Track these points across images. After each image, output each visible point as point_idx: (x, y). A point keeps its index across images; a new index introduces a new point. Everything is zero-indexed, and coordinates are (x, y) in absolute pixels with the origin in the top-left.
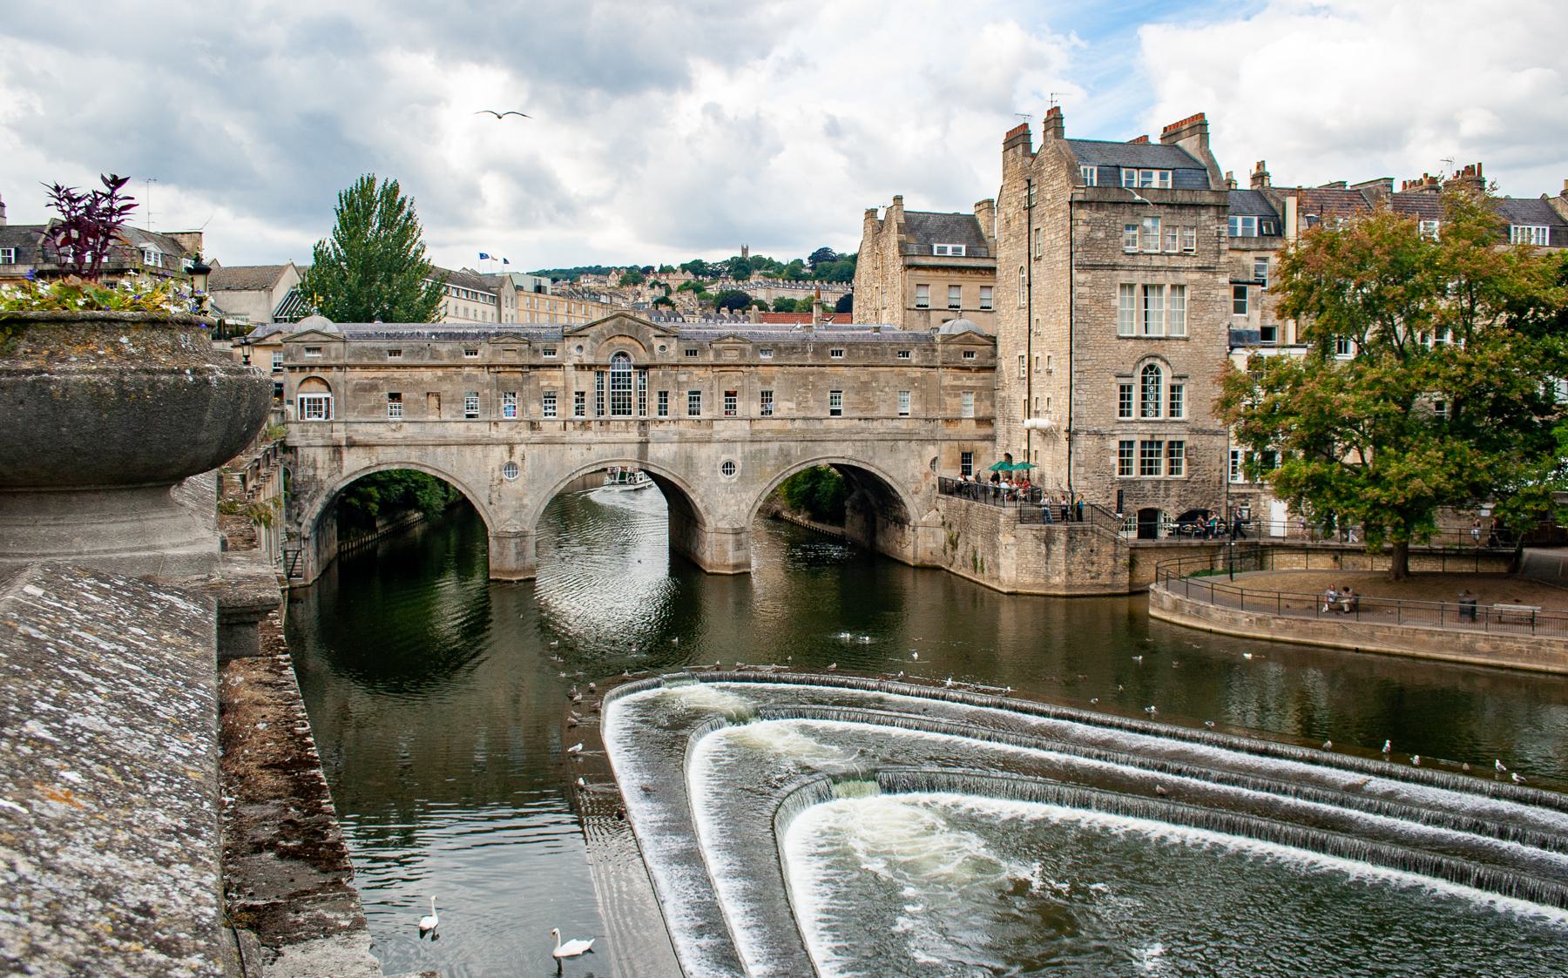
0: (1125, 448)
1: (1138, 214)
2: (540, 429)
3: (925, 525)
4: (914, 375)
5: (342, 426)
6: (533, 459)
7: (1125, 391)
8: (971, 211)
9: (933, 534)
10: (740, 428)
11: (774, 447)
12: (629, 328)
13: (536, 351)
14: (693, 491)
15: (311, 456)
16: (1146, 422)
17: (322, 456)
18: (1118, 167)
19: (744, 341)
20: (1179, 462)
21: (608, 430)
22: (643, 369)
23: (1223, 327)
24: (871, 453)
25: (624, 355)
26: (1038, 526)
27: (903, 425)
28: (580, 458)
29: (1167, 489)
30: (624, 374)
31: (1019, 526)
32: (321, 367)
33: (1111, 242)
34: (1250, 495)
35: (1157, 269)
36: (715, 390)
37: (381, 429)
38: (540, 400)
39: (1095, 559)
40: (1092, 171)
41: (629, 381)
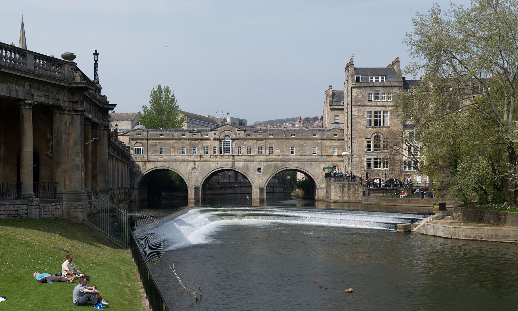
0: (369, 160)
1: (373, 90)
2: (203, 157)
3: (321, 188)
4: (318, 142)
6: (201, 166)
7: (369, 143)
8: (114, 110)
9: (323, 191)
10: (263, 158)
12: (229, 128)
14: (248, 176)
16: (375, 152)
20: (387, 165)
21: (223, 158)
24: (304, 166)
25: (228, 136)
26: (340, 183)
27: (314, 157)
28: (214, 166)
29: (382, 173)
30: (228, 141)
31: (335, 183)
32: (141, 139)
33: (364, 98)
35: (379, 106)
36: (255, 147)
37: (157, 157)
38: (203, 149)
39: (357, 192)
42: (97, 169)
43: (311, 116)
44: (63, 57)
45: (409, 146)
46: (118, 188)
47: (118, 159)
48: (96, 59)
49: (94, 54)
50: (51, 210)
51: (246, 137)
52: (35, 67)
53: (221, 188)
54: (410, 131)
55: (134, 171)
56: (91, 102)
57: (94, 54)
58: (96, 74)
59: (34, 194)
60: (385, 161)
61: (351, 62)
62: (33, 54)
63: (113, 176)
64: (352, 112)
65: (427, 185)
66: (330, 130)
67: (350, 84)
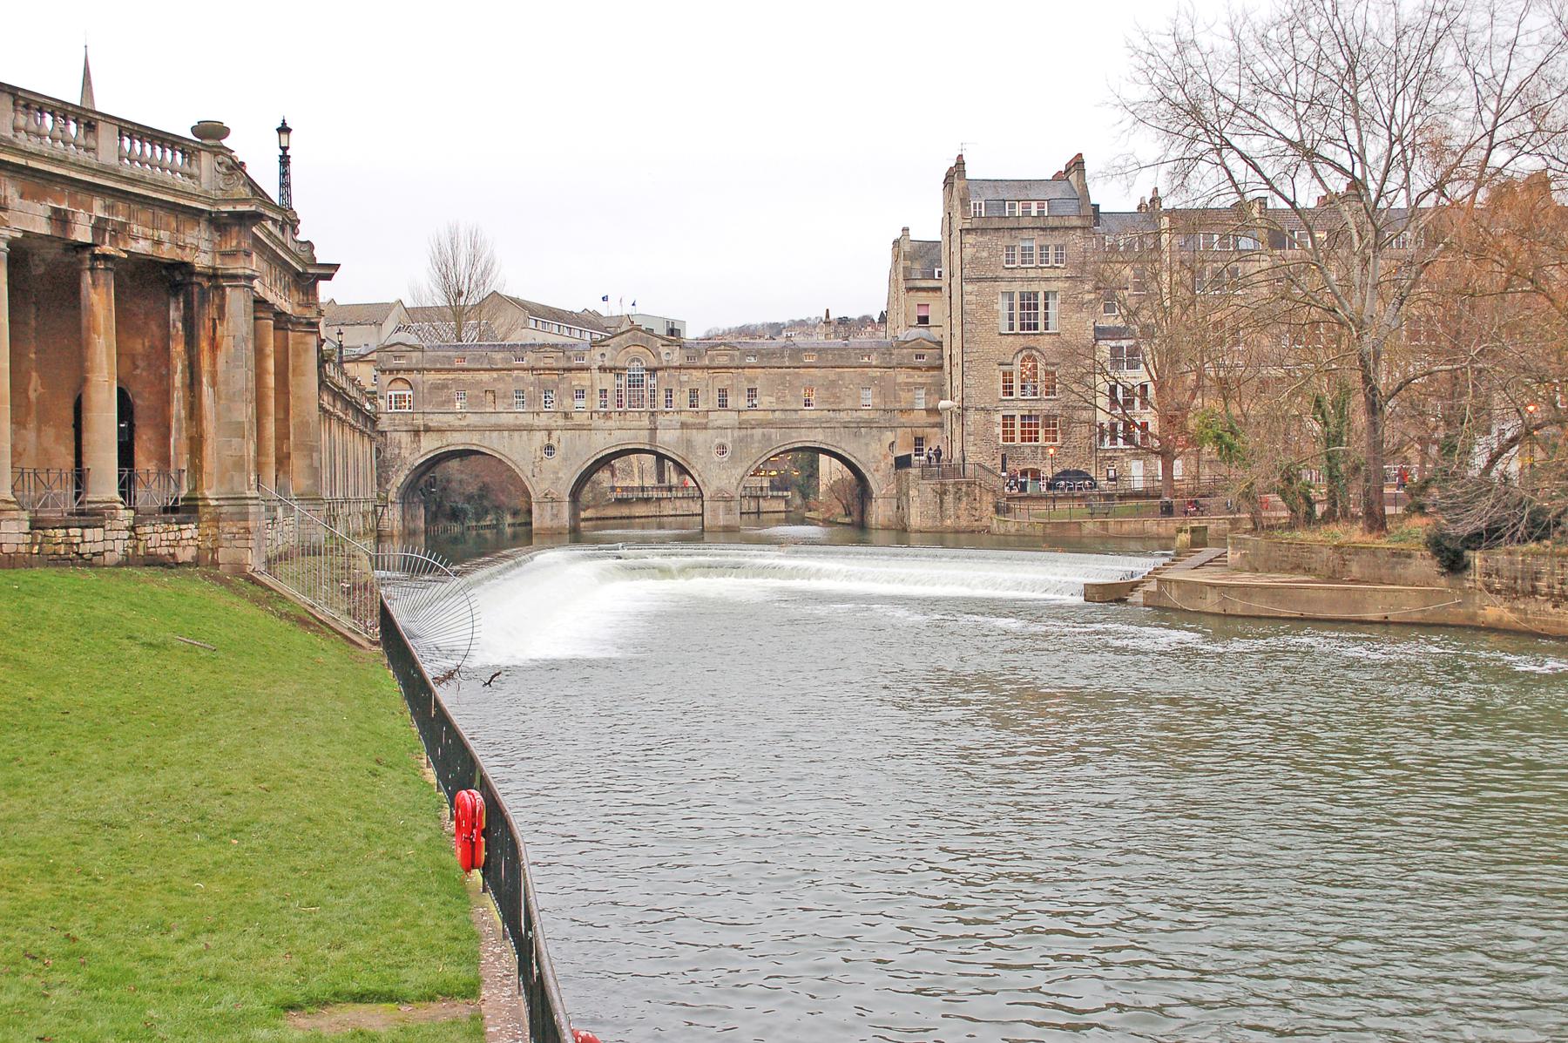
0: (1008, 420)
2: (572, 418)
5: (421, 415)
6: (566, 442)
7: (1008, 376)
10: (731, 418)
11: (758, 432)
12: (641, 339)
13: (569, 358)
15: (397, 438)
17: (406, 439)
18: (1004, 201)
19: (734, 348)
20: (1055, 432)
21: (625, 420)
22: (653, 371)
23: (1090, 323)
24: (838, 438)
25: (638, 360)
33: (993, 259)
34: (1115, 458)
35: (1032, 280)
36: (710, 388)
37: (450, 418)
40: (980, 204)
41: (642, 381)
42: (289, 439)
43: (855, 314)
44: (193, 129)
45: (1111, 383)
46: (347, 500)
47: (344, 421)
48: (284, 144)
49: (280, 130)
50: (168, 543)
51: (684, 362)
52: (121, 158)
53: (620, 501)
54: (1113, 344)
55: (388, 456)
56: (274, 259)
57: (280, 130)
58: (285, 185)
59: (122, 499)
60: (1050, 421)
61: (960, 163)
62: (115, 122)
63: (331, 467)
64: (964, 296)
65: (1157, 484)
66: (908, 342)
67: (958, 223)
